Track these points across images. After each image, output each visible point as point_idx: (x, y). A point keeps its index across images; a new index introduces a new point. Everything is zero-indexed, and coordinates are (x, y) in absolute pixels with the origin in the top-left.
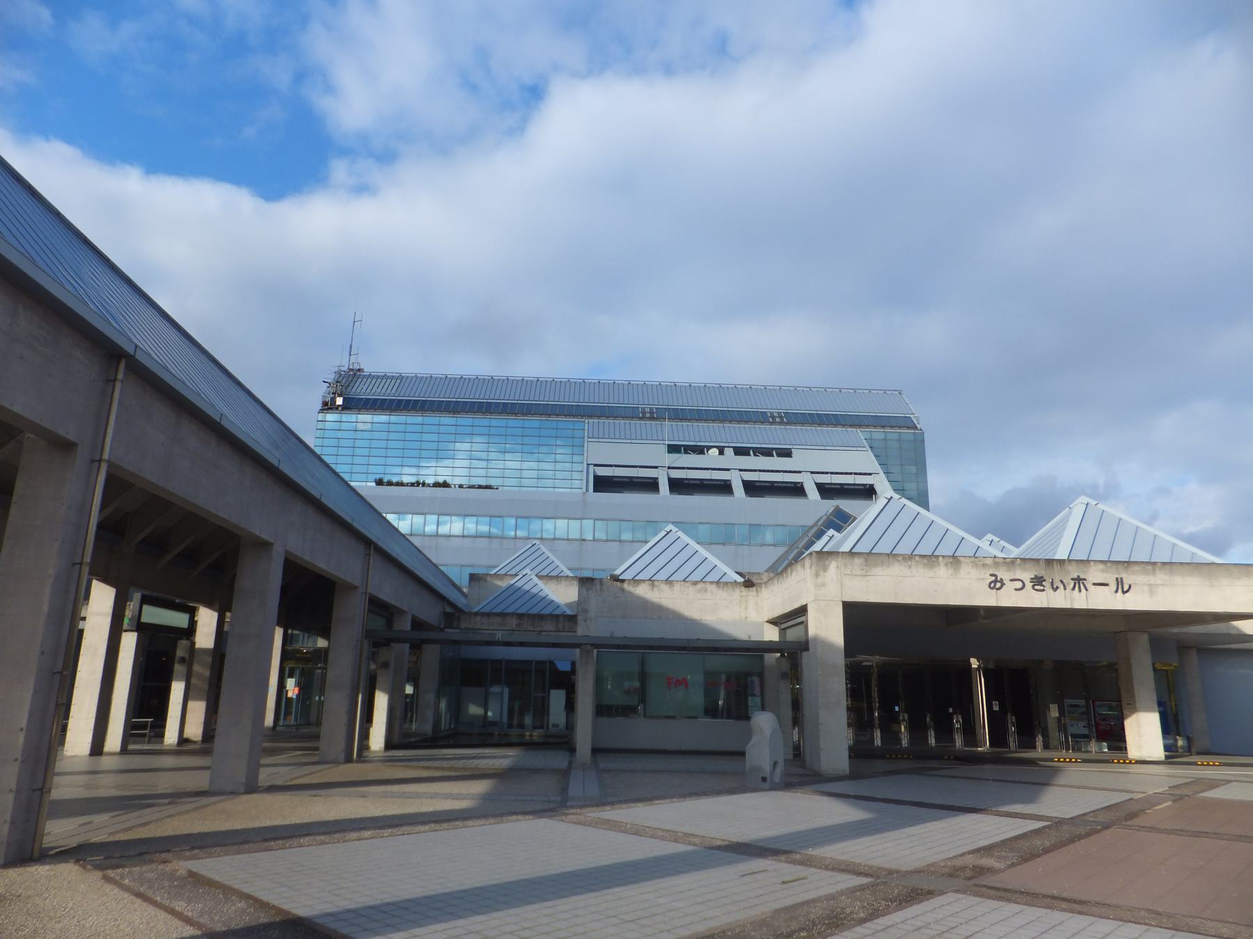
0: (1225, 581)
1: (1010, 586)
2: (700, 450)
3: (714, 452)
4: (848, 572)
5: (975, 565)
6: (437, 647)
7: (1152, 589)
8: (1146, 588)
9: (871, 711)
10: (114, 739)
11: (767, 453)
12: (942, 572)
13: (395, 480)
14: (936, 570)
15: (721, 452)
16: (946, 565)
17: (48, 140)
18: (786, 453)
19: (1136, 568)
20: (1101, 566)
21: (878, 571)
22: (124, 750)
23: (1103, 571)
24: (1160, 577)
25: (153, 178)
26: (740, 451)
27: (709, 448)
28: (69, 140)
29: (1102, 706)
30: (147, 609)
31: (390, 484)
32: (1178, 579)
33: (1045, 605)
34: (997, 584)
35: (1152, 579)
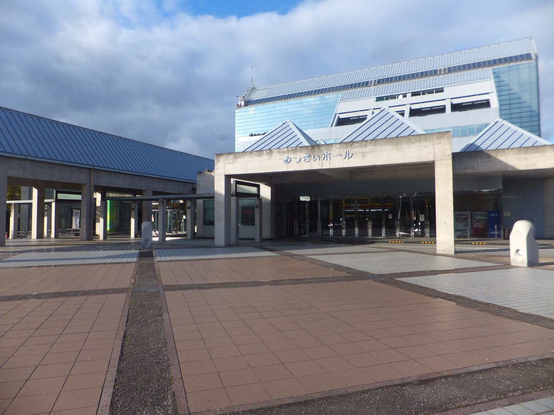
0: (405, 146)
1: (294, 161)
2: (393, 97)
3: (401, 96)
4: (227, 162)
5: (279, 152)
6: (202, 201)
7: (364, 154)
8: (361, 155)
9: (305, 219)
10: (53, 235)
11: (430, 92)
12: (265, 157)
13: (257, 133)
14: (262, 157)
15: (405, 96)
16: (267, 154)
17: (202, 16)
18: (441, 90)
19: (357, 144)
20: (338, 146)
21: (239, 160)
22: (533, 263)
23: (339, 148)
24: (370, 148)
25: (241, 19)
26: (414, 94)
27: (398, 95)
28: (209, 14)
29: (476, 214)
30: (59, 195)
31: (255, 135)
32: (379, 148)
33: (309, 169)
34: (287, 162)
35: (364, 150)
